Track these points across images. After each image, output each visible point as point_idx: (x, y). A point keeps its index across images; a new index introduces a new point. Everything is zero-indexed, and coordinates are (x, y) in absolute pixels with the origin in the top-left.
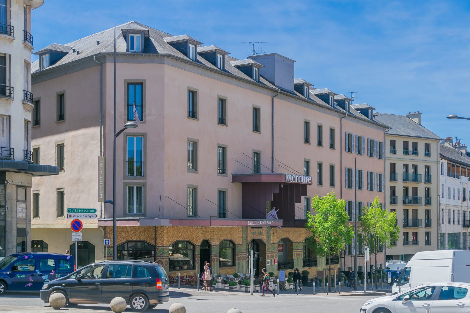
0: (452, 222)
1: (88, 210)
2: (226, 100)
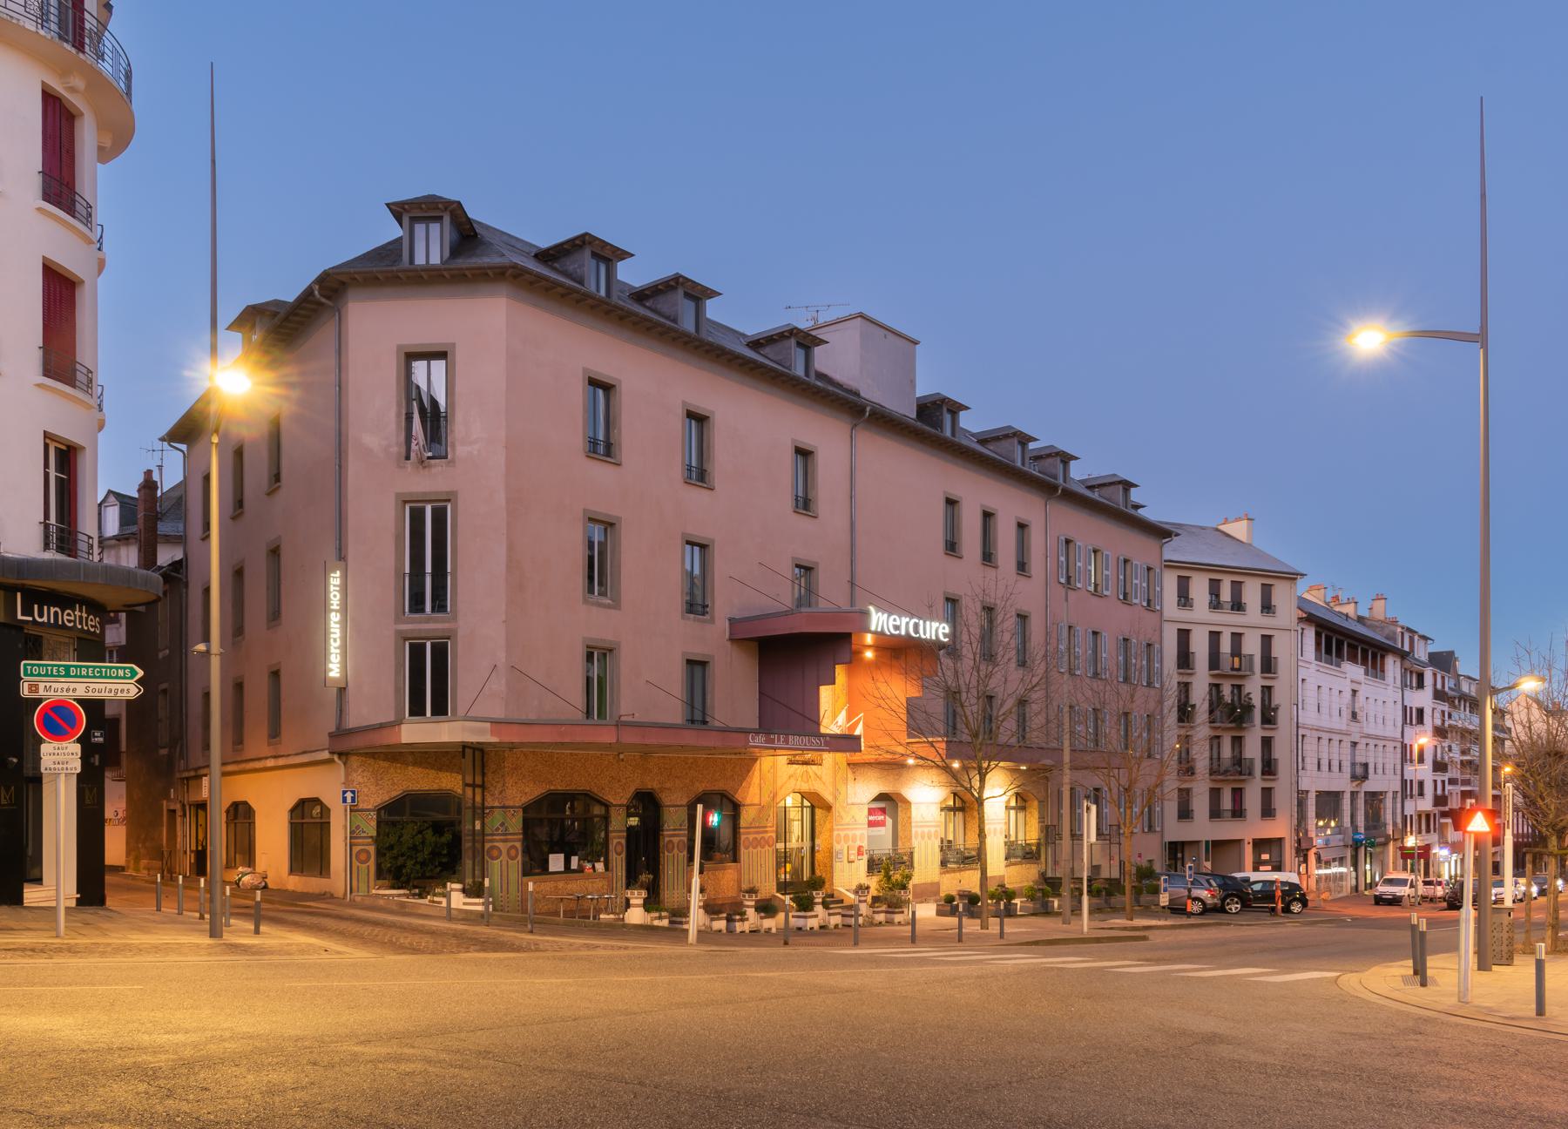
0: (1325, 767)
2: (711, 419)
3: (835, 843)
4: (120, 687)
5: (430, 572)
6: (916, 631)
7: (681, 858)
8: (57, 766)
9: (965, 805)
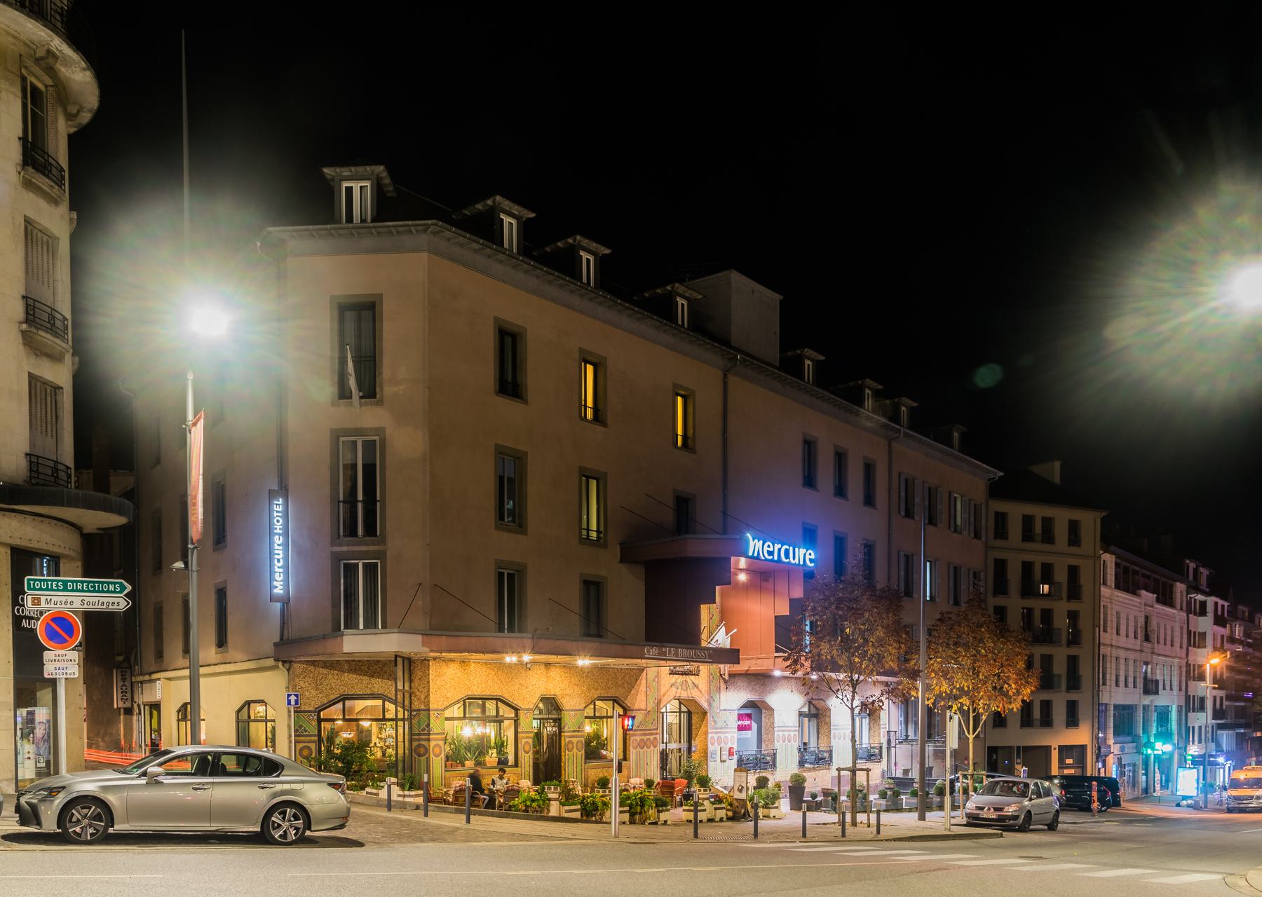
0: (1122, 683)
1: (97, 585)
3: (709, 745)
4: (111, 600)
5: (361, 499)
6: (787, 556)
7: (579, 757)
8: (58, 671)
9: (816, 714)
